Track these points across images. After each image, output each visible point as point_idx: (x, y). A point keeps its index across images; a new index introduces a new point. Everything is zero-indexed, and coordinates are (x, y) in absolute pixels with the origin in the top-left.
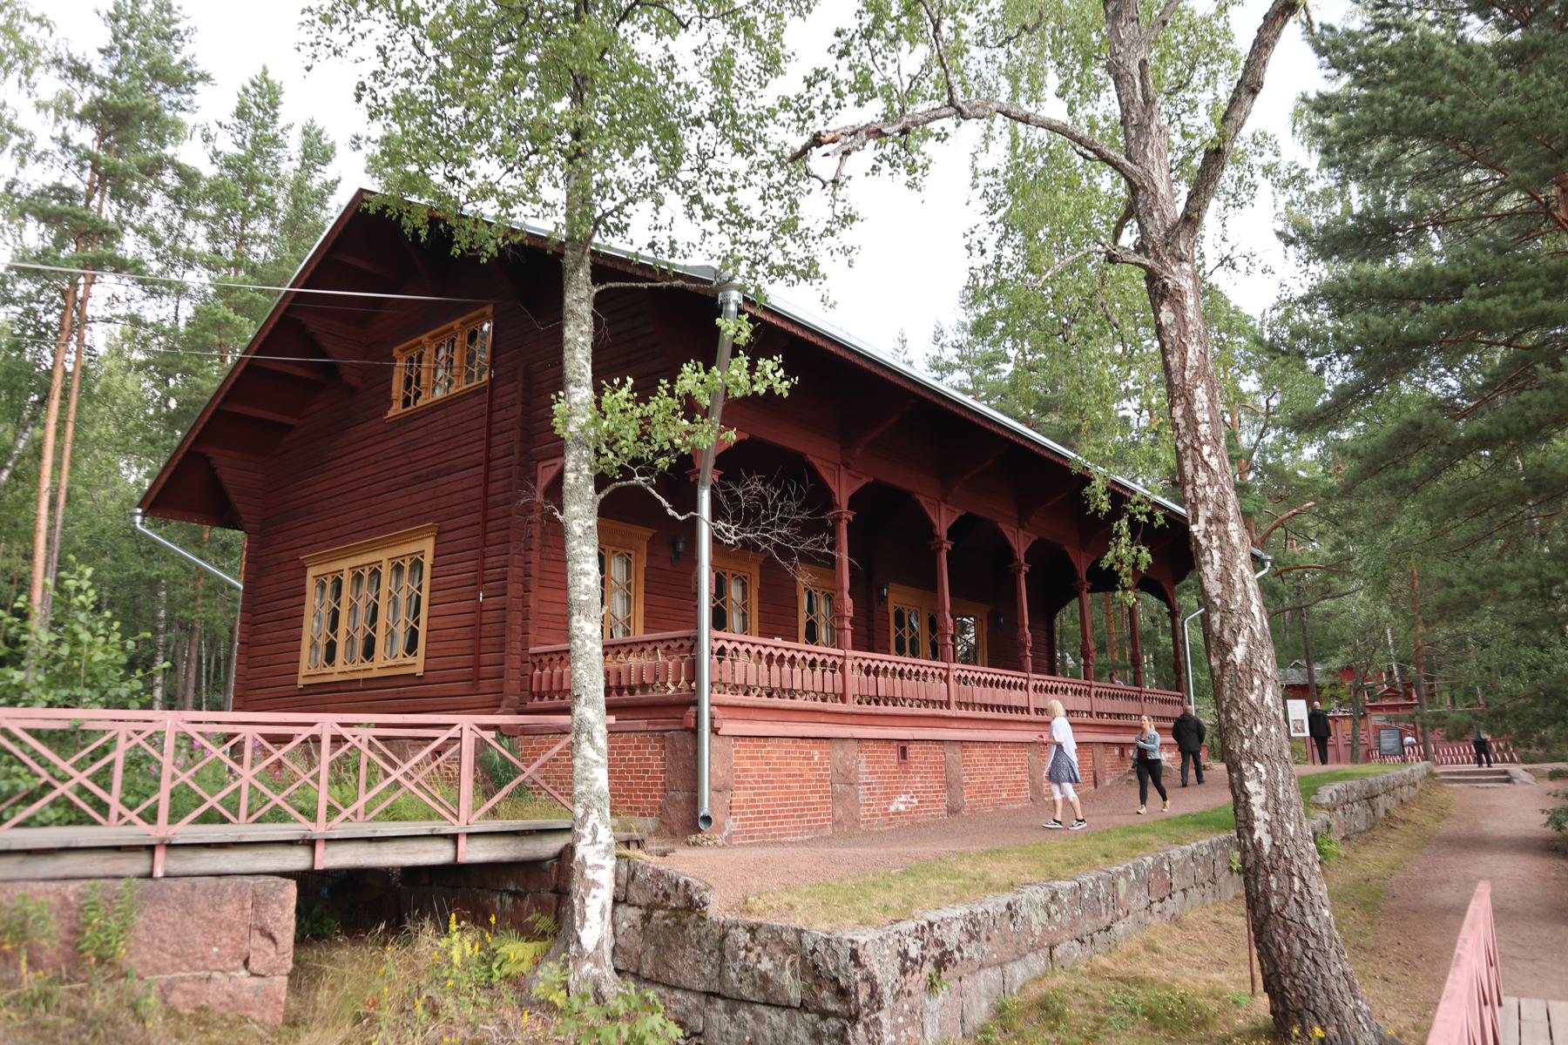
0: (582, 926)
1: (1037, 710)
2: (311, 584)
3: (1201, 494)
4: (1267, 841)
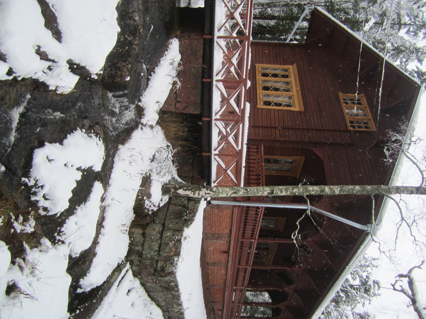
0: (183, 190)
1: (242, 242)
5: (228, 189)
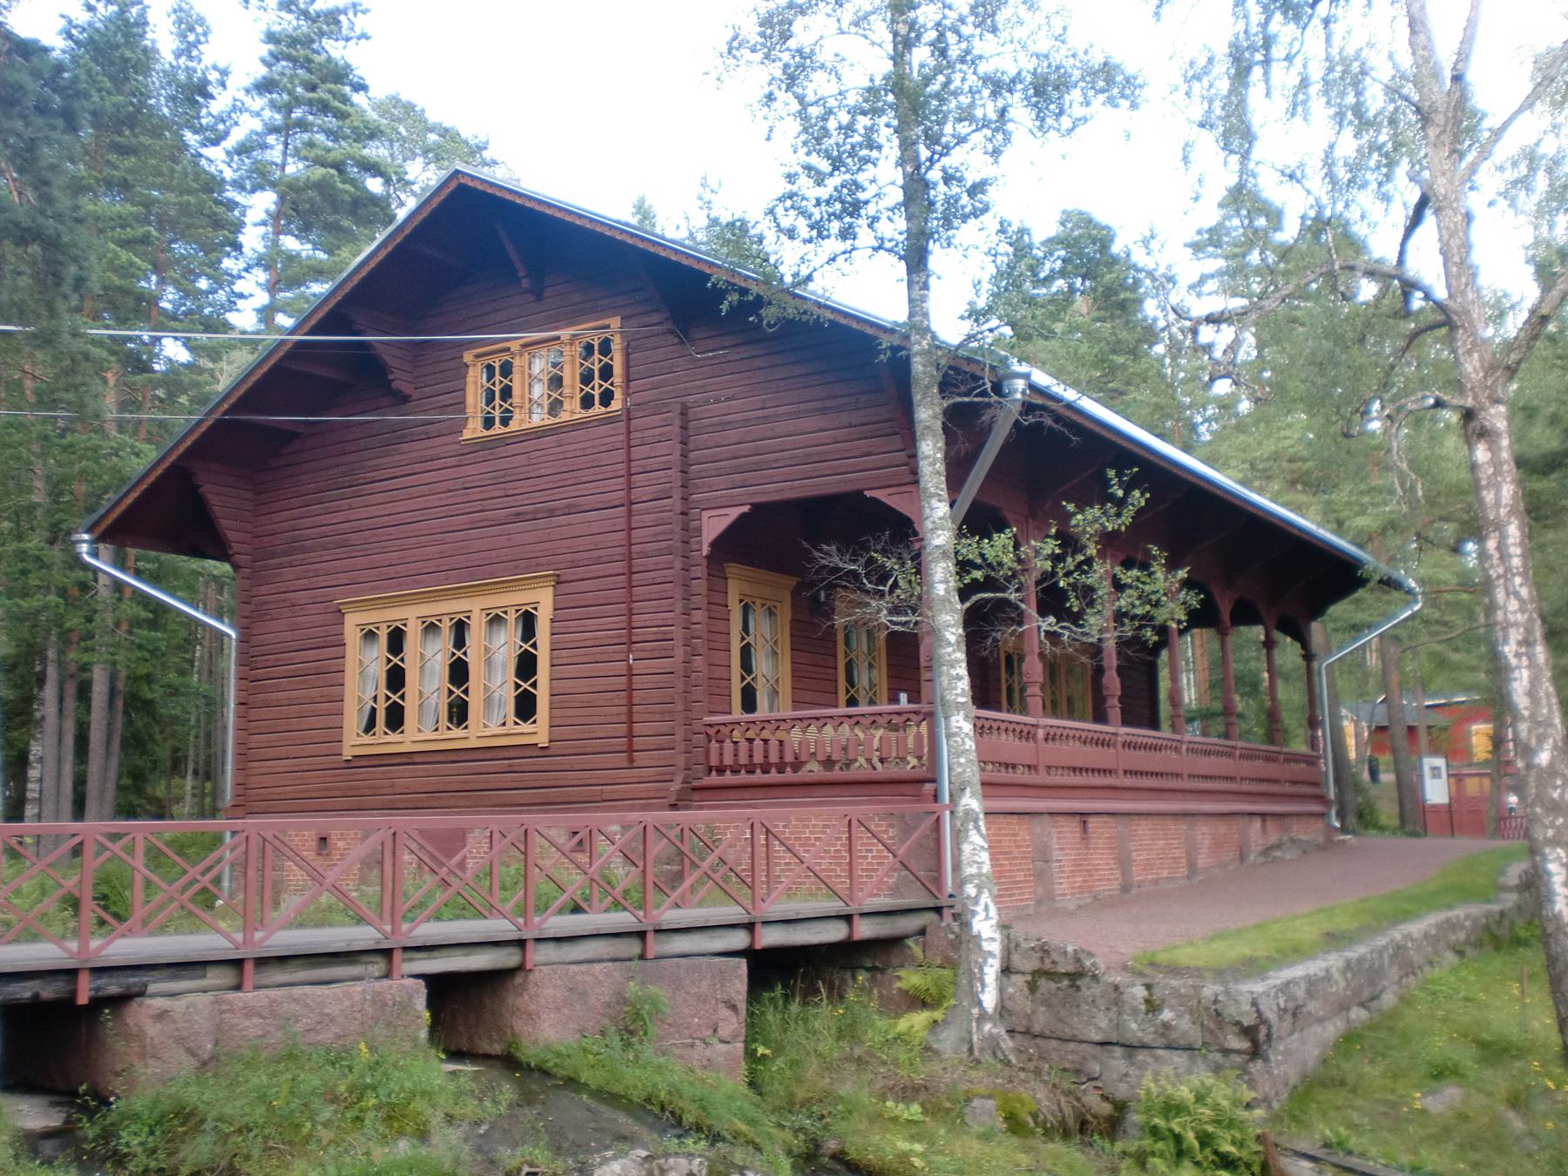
0: (983, 991)
2: (352, 634)
5: (966, 848)
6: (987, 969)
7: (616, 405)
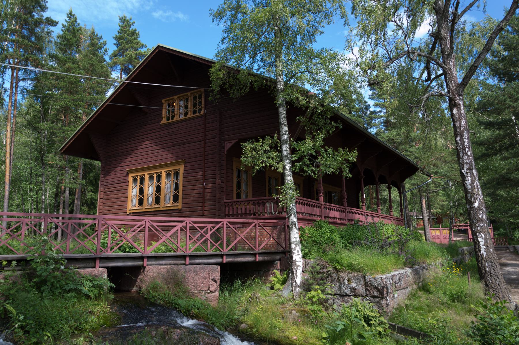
3: (465, 162)
4: (485, 254)
6: (298, 271)
7: (202, 112)
